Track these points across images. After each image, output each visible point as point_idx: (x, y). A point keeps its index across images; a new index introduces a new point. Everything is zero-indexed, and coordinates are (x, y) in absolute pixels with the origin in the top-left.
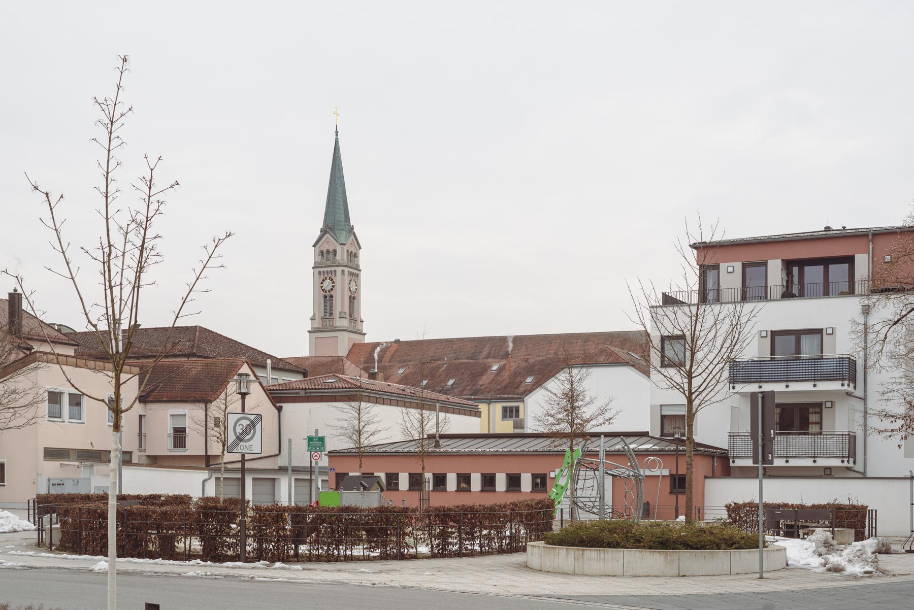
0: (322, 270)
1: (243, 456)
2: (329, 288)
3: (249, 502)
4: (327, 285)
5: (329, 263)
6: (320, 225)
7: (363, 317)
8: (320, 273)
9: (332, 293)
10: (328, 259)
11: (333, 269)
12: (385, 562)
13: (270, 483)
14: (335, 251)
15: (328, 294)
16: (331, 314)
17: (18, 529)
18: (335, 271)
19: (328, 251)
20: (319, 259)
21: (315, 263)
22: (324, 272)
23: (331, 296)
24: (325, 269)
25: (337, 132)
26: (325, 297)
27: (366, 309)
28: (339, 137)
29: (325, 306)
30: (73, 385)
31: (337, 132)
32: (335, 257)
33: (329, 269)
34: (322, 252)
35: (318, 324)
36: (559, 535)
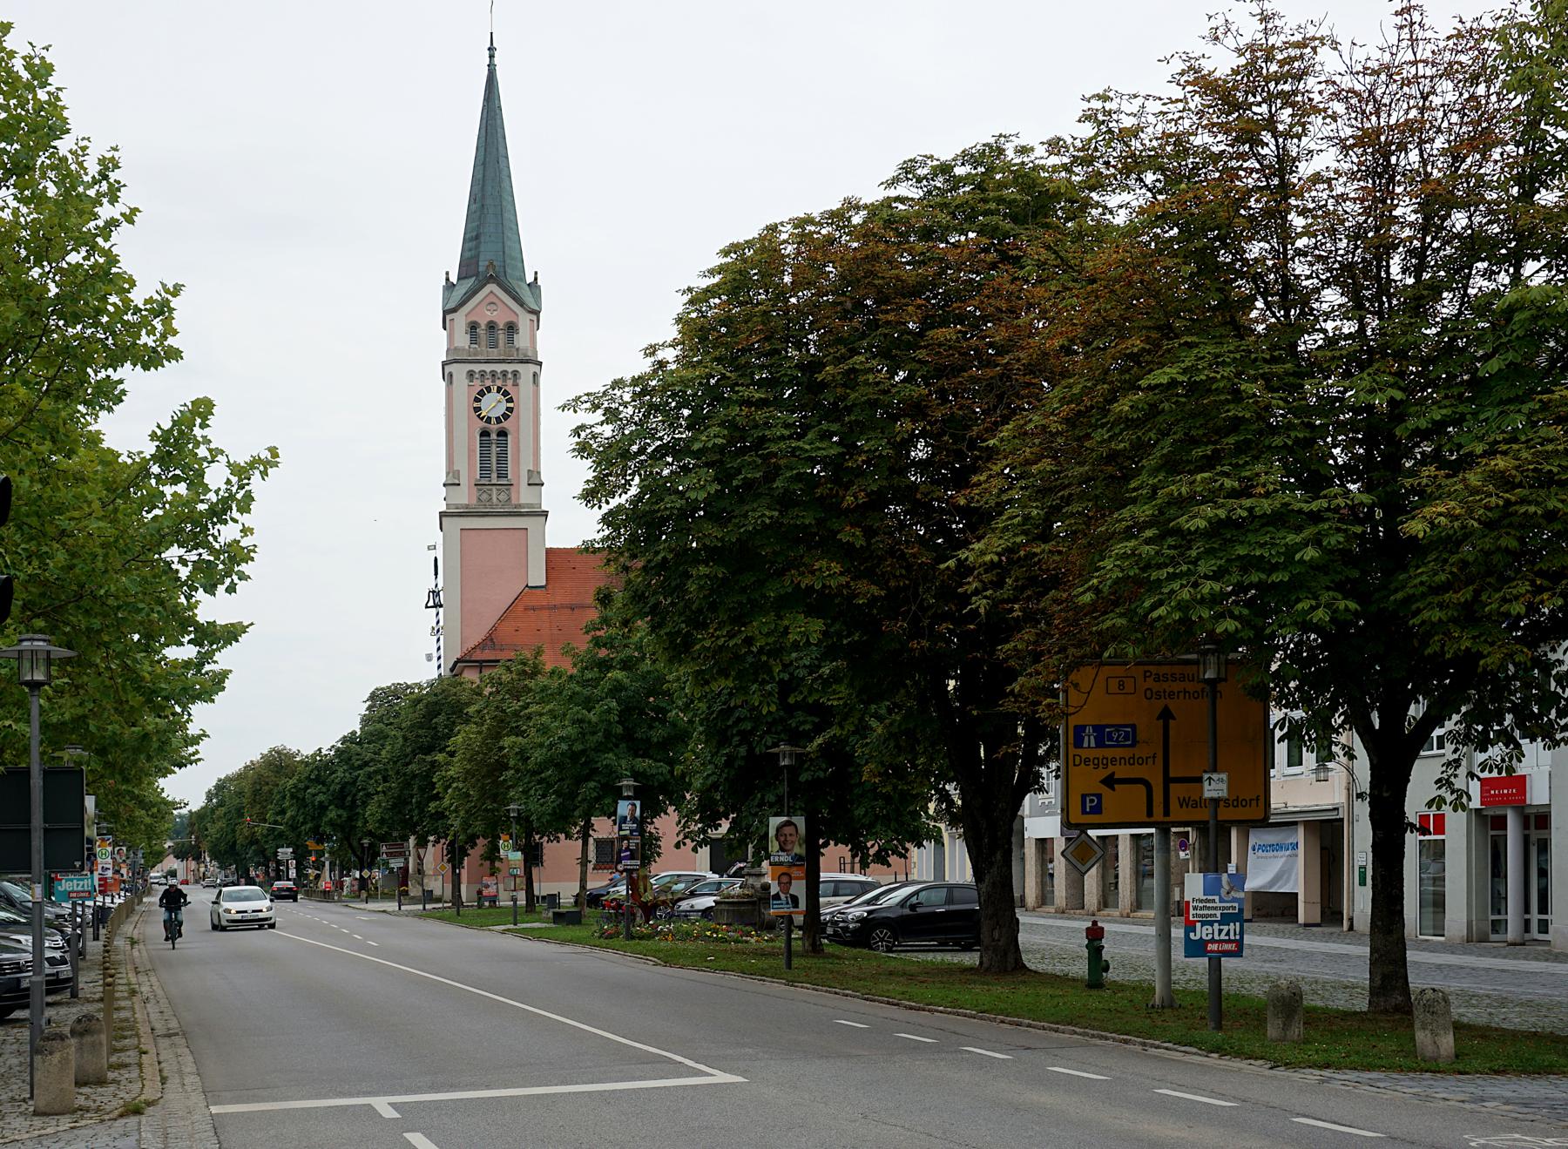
0: (477, 368)
1: (789, 966)
3: (96, 217)
4: (493, 405)
5: (494, 353)
6: (450, 261)
7: (294, 750)
8: (471, 374)
9: (505, 424)
11: (510, 368)
17: (568, 611)
18: (515, 373)
19: (492, 326)
22: (483, 374)
23: (503, 433)
24: (488, 368)
25: (491, 49)
26: (485, 433)
28: (496, 60)
29: (484, 457)
31: (491, 49)
35: (464, 496)
36: (151, 784)
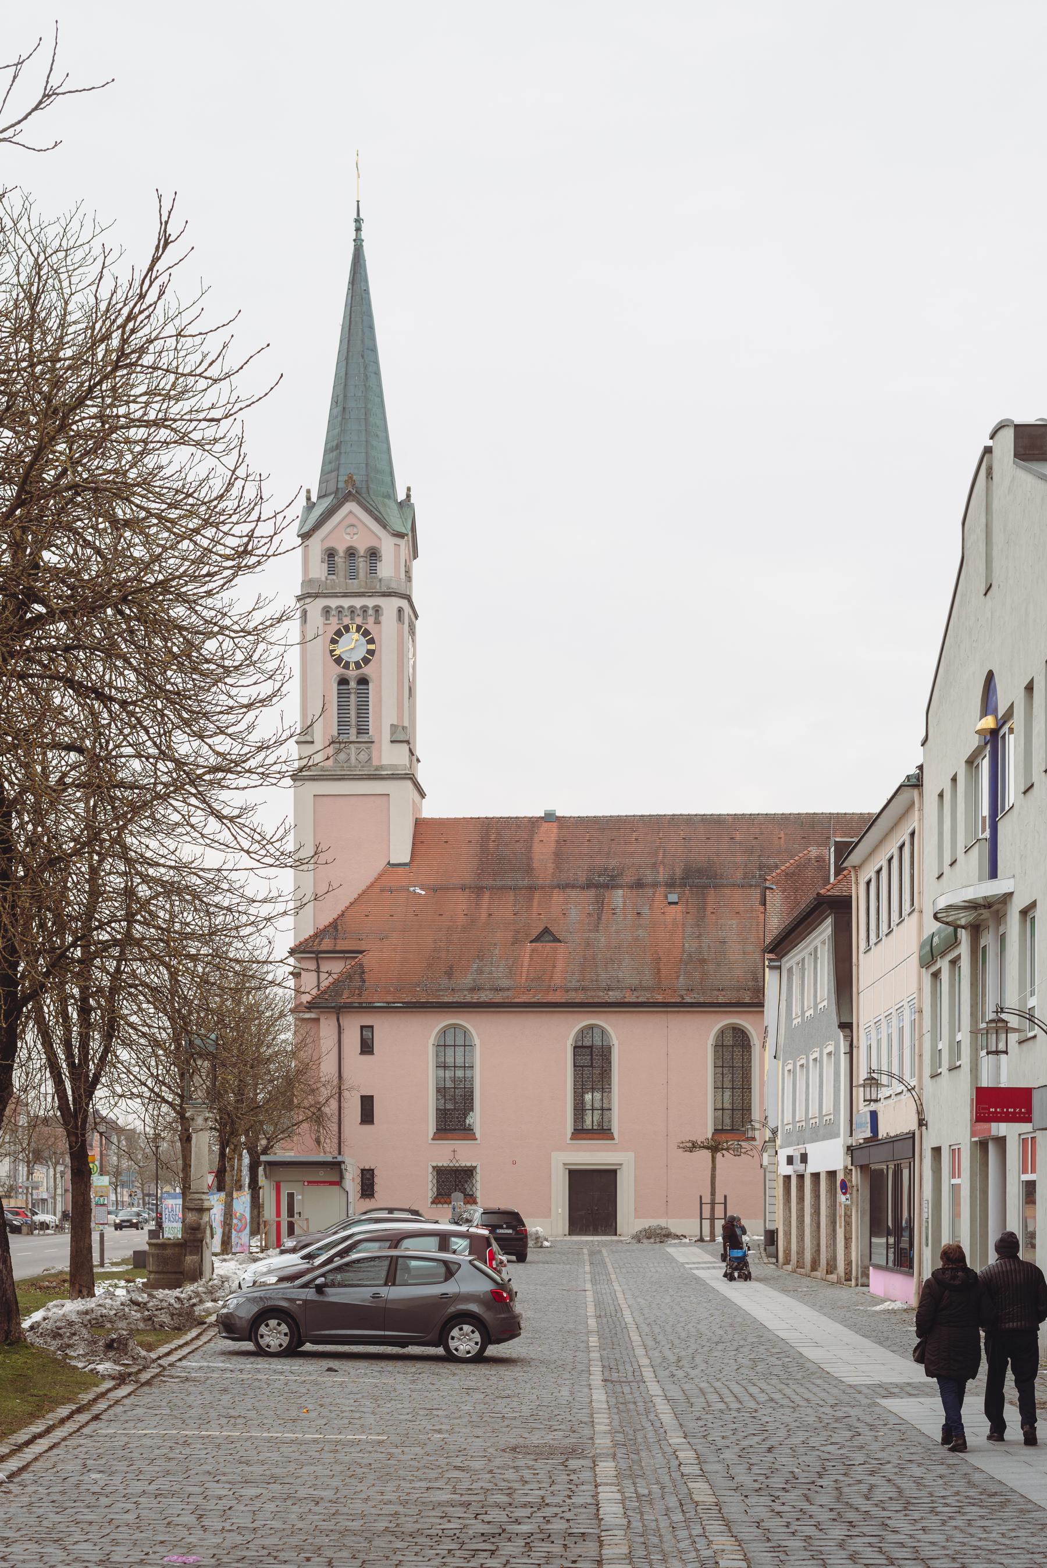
0: (333, 603)
2: (358, 655)
5: (354, 586)
8: (327, 611)
9: (366, 670)
10: (353, 574)
11: (370, 602)
12: (287, 1361)
13: (351, 516)
14: (374, 554)
15: (352, 673)
16: (362, 731)
18: (377, 609)
19: (351, 553)
20: (319, 571)
21: (307, 582)
22: (340, 610)
23: (363, 681)
24: (346, 603)
25: (358, 221)
26: (343, 681)
27: (14, 1273)
28: (364, 234)
30: (170, 213)
31: (358, 221)
32: (373, 570)
33: (358, 603)
34: (330, 554)
